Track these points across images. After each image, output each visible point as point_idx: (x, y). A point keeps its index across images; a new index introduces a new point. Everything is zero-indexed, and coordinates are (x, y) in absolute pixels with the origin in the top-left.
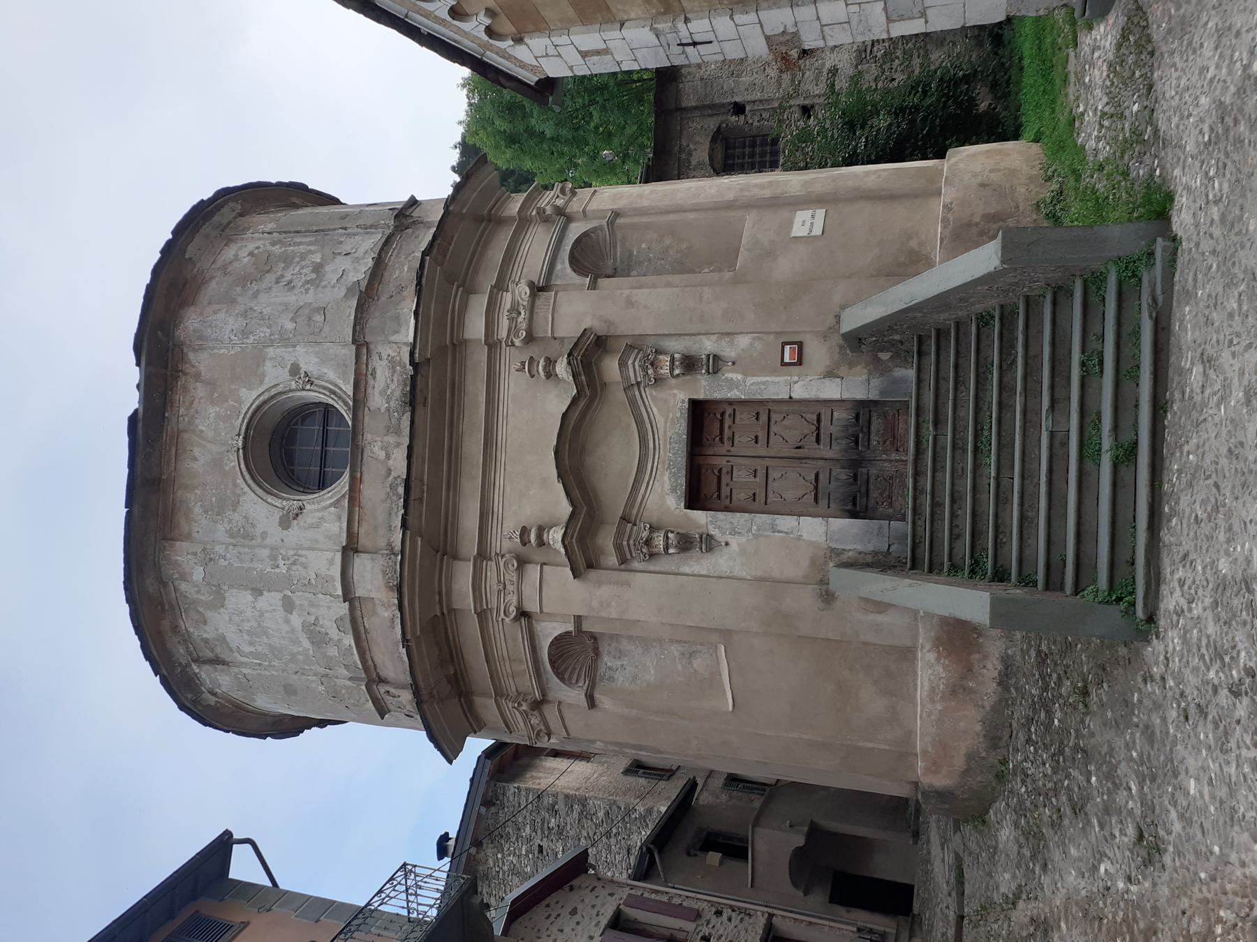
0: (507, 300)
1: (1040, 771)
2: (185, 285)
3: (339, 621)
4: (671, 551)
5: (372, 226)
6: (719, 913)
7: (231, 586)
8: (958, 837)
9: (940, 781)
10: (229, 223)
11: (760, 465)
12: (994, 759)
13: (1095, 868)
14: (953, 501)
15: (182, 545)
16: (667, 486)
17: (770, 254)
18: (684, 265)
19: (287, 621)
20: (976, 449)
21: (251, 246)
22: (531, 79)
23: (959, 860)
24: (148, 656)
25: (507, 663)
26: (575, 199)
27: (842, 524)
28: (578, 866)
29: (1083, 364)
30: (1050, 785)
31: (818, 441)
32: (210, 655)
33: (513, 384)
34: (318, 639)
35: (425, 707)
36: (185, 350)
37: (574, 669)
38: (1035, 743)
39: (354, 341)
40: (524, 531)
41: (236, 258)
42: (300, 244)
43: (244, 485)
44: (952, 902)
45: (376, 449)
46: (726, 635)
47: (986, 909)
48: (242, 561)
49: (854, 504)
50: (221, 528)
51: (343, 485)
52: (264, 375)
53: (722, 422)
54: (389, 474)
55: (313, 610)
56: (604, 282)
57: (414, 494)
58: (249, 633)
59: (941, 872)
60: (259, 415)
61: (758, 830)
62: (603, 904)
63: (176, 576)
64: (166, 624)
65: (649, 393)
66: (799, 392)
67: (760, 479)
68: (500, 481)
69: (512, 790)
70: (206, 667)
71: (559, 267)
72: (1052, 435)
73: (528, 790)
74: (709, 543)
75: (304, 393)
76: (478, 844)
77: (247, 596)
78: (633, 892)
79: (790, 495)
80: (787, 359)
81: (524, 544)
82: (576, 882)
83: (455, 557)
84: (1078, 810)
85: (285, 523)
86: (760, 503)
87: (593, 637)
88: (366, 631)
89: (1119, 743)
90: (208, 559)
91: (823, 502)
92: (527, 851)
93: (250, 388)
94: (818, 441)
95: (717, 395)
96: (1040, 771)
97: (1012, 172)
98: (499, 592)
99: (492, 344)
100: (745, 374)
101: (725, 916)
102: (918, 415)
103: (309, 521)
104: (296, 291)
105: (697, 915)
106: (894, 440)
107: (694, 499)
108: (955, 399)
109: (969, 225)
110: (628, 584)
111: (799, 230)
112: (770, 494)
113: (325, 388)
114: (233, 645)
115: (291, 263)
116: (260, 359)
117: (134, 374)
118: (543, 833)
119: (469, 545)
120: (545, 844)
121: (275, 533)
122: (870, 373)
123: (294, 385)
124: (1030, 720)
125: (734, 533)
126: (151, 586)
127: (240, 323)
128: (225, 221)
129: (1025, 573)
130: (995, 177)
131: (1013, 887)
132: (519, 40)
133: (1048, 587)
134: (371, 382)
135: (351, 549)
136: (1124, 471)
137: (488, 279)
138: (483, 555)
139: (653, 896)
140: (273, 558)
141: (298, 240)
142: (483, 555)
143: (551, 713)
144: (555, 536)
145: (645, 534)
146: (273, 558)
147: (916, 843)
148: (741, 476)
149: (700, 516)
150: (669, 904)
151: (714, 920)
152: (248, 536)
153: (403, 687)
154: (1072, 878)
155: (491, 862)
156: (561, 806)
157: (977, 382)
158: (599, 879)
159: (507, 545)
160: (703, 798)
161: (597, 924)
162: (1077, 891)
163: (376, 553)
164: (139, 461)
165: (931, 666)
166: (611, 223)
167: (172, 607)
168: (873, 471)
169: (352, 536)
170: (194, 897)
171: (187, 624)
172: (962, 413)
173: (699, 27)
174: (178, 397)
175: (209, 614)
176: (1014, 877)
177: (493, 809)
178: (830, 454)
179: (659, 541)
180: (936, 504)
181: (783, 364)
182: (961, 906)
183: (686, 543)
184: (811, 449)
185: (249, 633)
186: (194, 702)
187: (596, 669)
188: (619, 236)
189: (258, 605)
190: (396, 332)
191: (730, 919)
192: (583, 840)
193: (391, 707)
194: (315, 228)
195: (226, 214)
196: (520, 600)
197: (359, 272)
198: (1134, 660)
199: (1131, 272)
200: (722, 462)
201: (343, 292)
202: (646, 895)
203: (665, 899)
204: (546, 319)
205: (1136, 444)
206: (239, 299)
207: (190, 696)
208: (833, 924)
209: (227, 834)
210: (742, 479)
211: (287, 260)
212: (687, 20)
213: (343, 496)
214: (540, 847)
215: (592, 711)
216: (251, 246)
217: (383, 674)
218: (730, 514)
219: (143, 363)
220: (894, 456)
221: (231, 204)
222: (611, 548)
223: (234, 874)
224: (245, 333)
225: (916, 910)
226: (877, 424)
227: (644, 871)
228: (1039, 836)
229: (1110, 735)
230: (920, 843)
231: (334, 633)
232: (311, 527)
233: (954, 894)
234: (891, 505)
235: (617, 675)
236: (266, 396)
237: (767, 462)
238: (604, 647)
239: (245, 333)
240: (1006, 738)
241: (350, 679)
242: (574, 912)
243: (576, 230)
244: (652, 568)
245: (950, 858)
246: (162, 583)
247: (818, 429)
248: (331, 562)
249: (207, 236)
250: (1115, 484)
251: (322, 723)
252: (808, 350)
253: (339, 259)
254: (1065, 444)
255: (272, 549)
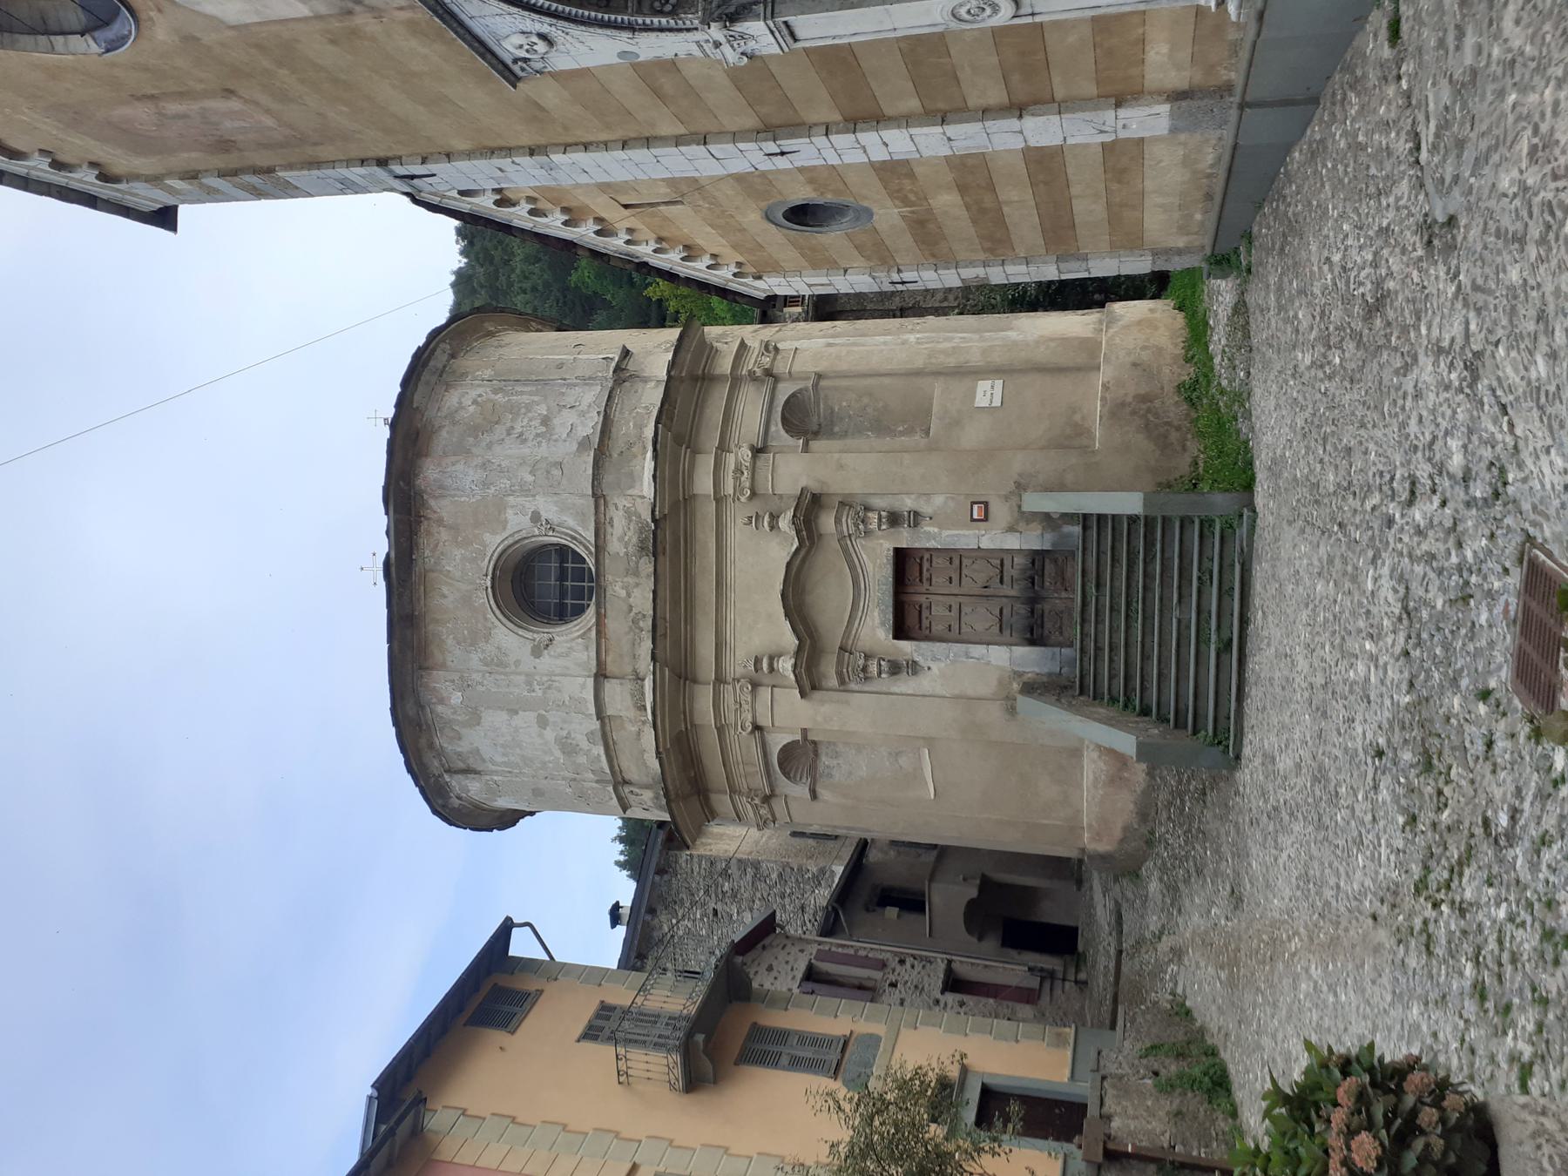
0: (731, 460)
1: (1177, 842)
2: (418, 434)
3: (590, 736)
4: (883, 676)
5: (590, 378)
6: (902, 962)
7: (489, 708)
8: (1117, 888)
9: (1103, 847)
10: (445, 367)
11: (954, 601)
12: (1144, 830)
13: (1209, 911)
14: (1111, 650)
15: (438, 674)
16: (877, 621)
17: (955, 423)
18: (881, 425)
19: (540, 735)
20: (1127, 616)
21: (473, 394)
22: (762, 295)
23: (1118, 905)
24: (410, 770)
25: (741, 766)
26: (779, 357)
27: (1023, 652)
28: (767, 927)
29: (1199, 578)
30: (1183, 853)
31: (1002, 582)
32: (461, 765)
33: (739, 533)
34: (568, 747)
35: (673, 805)
36: (425, 497)
37: (797, 768)
38: (1174, 822)
39: (594, 495)
40: (758, 661)
41: (461, 407)
42: (522, 393)
43: (494, 619)
44: (1113, 940)
45: (617, 588)
46: (930, 742)
47: (1139, 943)
48: (499, 686)
49: (1032, 634)
50: (475, 659)
51: (590, 615)
52: (506, 521)
53: (921, 565)
54: (631, 610)
55: (565, 726)
56: (814, 444)
57: (660, 631)
58: (502, 746)
59: (1103, 915)
60: (504, 558)
61: (934, 885)
62: (796, 960)
63: (434, 700)
64: (423, 742)
65: (860, 544)
66: (986, 544)
67: (955, 612)
68: (730, 616)
69: (684, 857)
70: (456, 777)
71: (773, 428)
72: (1179, 621)
73: (700, 857)
74: (914, 668)
75: (546, 538)
76: (652, 911)
77: (504, 716)
78: (821, 947)
79: (979, 627)
80: (975, 516)
81: (756, 671)
82: (767, 941)
83: (695, 681)
84: (1199, 872)
85: (537, 652)
86: (954, 635)
87: (814, 743)
88: (614, 743)
89: (1222, 831)
90: (465, 685)
91: (1007, 632)
92: (702, 915)
93: (494, 533)
94: (1002, 582)
95: (917, 545)
96: (1177, 842)
97: (1159, 350)
98: (736, 710)
99: (719, 499)
100: (940, 528)
101: (908, 965)
102: (1083, 576)
103: (559, 650)
104: (530, 444)
105: (882, 965)
106: (1063, 581)
107: (900, 632)
108: (1112, 574)
109: (1123, 405)
110: (847, 703)
111: (981, 401)
112: (963, 626)
113: (566, 534)
114: (486, 757)
115: (518, 415)
116: (501, 507)
117: (381, 521)
118: (717, 896)
119: (706, 668)
120: (719, 907)
121: (528, 662)
122: (1044, 528)
123: (537, 532)
124: (1170, 804)
125: (935, 659)
126: (411, 710)
127: (479, 475)
128: (440, 366)
129: (1162, 712)
130: (1145, 356)
131: (1159, 925)
132: (759, 278)
133: (1176, 726)
134: (609, 530)
135: (601, 675)
136: (1224, 657)
137: (711, 440)
138: (720, 680)
139: (840, 950)
140: (529, 683)
141: (519, 389)
142: (720, 680)
143: (779, 806)
144: (786, 665)
145: (861, 662)
146: (529, 683)
147: (1079, 889)
148: (938, 611)
149: (906, 646)
150: (856, 955)
151: (898, 968)
152: (501, 664)
153: (647, 787)
154: (1196, 918)
155: (666, 929)
156: (733, 870)
157: (1128, 560)
158: (787, 937)
159: (740, 671)
160: (873, 856)
161: (794, 978)
162: (1199, 928)
163: (623, 678)
164: (394, 601)
165: (1094, 762)
166: (816, 386)
167: (428, 726)
168: (1047, 607)
169: (600, 663)
170: (489, 973)
171: (441, 741)
172: (1117, 584)
173: (907, 276)
174: (423, 540)
175: (464, 731)
176: (1160, 918)
177: (666, 877)
178: (1013, 593)
179: (874, 669)
180: (1098, 649)
181: (973, 520)
182: (1120, 942)
183: (895, 669)
184: (996, 588)
185: (502, 746)
186: (443, 806)
187: (816, 768)
188: (822, 396)
189: (513, 724)
190: (631, 487)
191: (913, 967)
192: (757, 902)
193: (632, 803)
194: (534, 378)
195: (440, 359)
196: (754, 717)
197: (589, 426)
198: (1230, 779)
199: (1229, 529)
200: (922, 599)
201: (575, 446)
202: (833, 949)
203: (851, 952)
204: (767, 478)
205: (1231, 640)
206: (474, 450)
207: (440, 802)
208: (1007, 966)
209: (508, 920)
210: (939, 613)
211: (514, 410)
212: (899, 271)
213: (590, 629)
214: (715, 912)
215: (815, 804)
216: (473, 394)
217: (627, 777)
218: (930, 643)
219: (391, 512)
220: (1064, 595)
221: (442, 346)
222: (833, 671)
223: (513, 951)
224: (486, 484)
225: (1080, 948)
226: (1049, 568)
227: (830, 927)
228: (1176, 889)
229: (1218, 823)
230: (1083, 890)
231: (584, 744)
232: (560, 656)
233: (1114, 934)
234: (1061, 633)
235: (834, 772)
236: (511, 541)
237: (961, 599)
238: (823, 750)
239: (486, 484)
240: (1153, 813)
241: (597, 782)
242: (770, 969)
243: (785, 391)
244: (866, 689)
245: (1110, 905)
246: (420, 706)
247: (1002, 572)
248: (583, 686)
249: (427, 383)
250: (1218, 666)
251: (532, 814)
252: (992, 508)
253: (565, 412)
254: (1189, 627)
255: (527, 675)
